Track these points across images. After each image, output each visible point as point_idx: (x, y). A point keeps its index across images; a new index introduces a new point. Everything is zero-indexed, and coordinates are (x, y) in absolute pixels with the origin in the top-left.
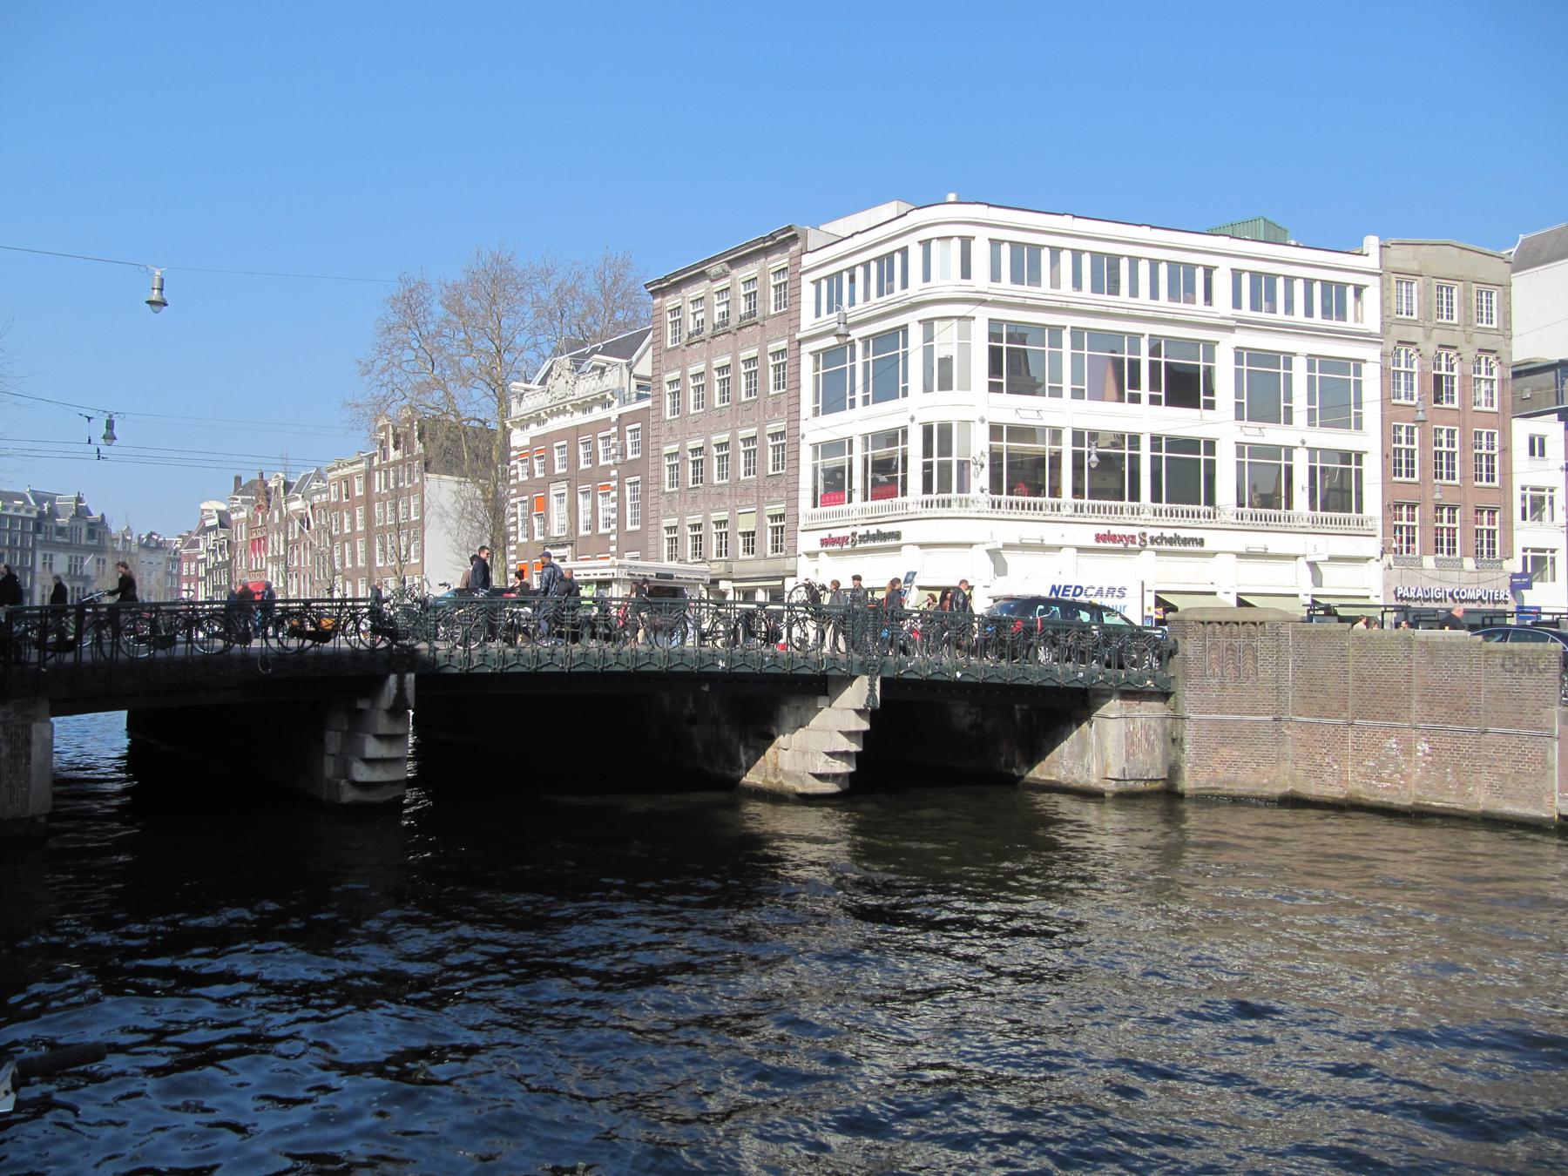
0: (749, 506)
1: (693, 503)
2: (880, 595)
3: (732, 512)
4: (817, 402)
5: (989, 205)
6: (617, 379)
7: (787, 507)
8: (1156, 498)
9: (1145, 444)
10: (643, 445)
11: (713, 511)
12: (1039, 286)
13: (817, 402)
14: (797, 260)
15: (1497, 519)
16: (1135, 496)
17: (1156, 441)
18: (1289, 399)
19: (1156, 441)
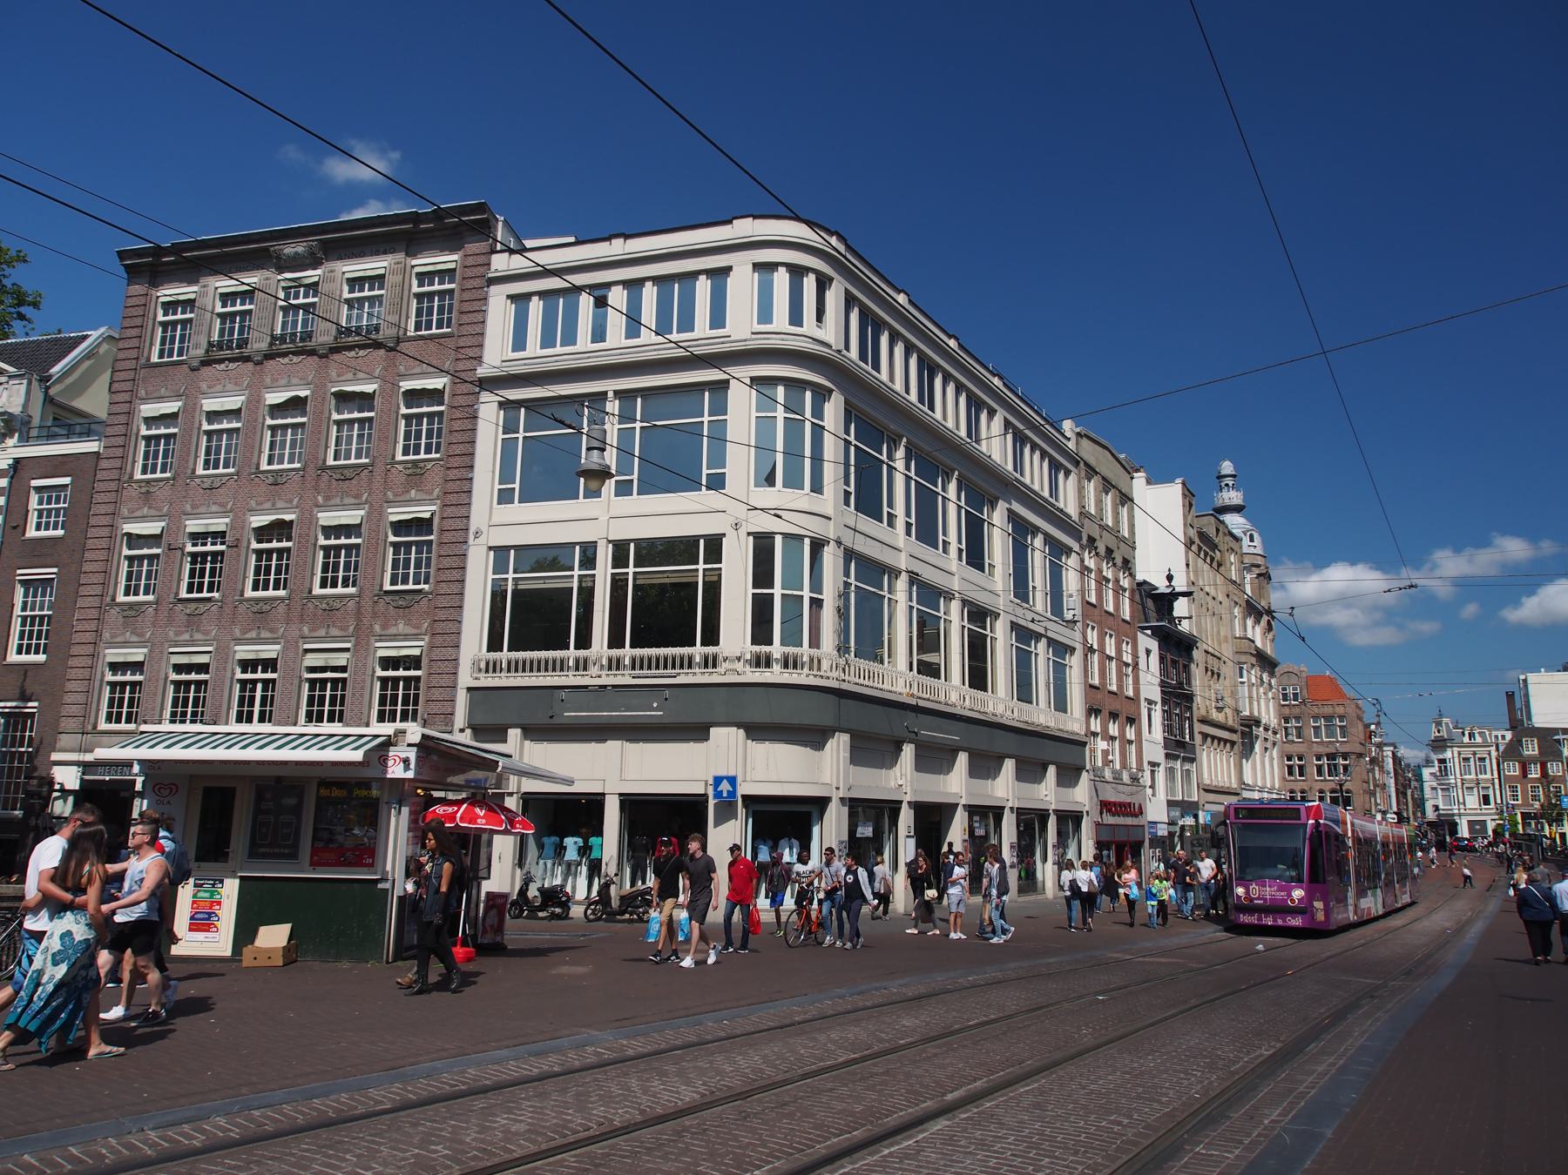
0: (335, 639)
1: (188, 625)
2: (88, 805)
3: (290, 645)
4: (847, 483)
5: (755, 217)
6: (21, 400)
7: (432, 647)
8: (616, 641)
9: (604, 556)
10: (76, 519)
11: (239, 641)
12: (758, 323)
13: (847, 483)
14: (481, 260)
15: (32, 658)
16: (584, 641)
17: (620, 551)
18: (890, 505)
19: (620, 551)
